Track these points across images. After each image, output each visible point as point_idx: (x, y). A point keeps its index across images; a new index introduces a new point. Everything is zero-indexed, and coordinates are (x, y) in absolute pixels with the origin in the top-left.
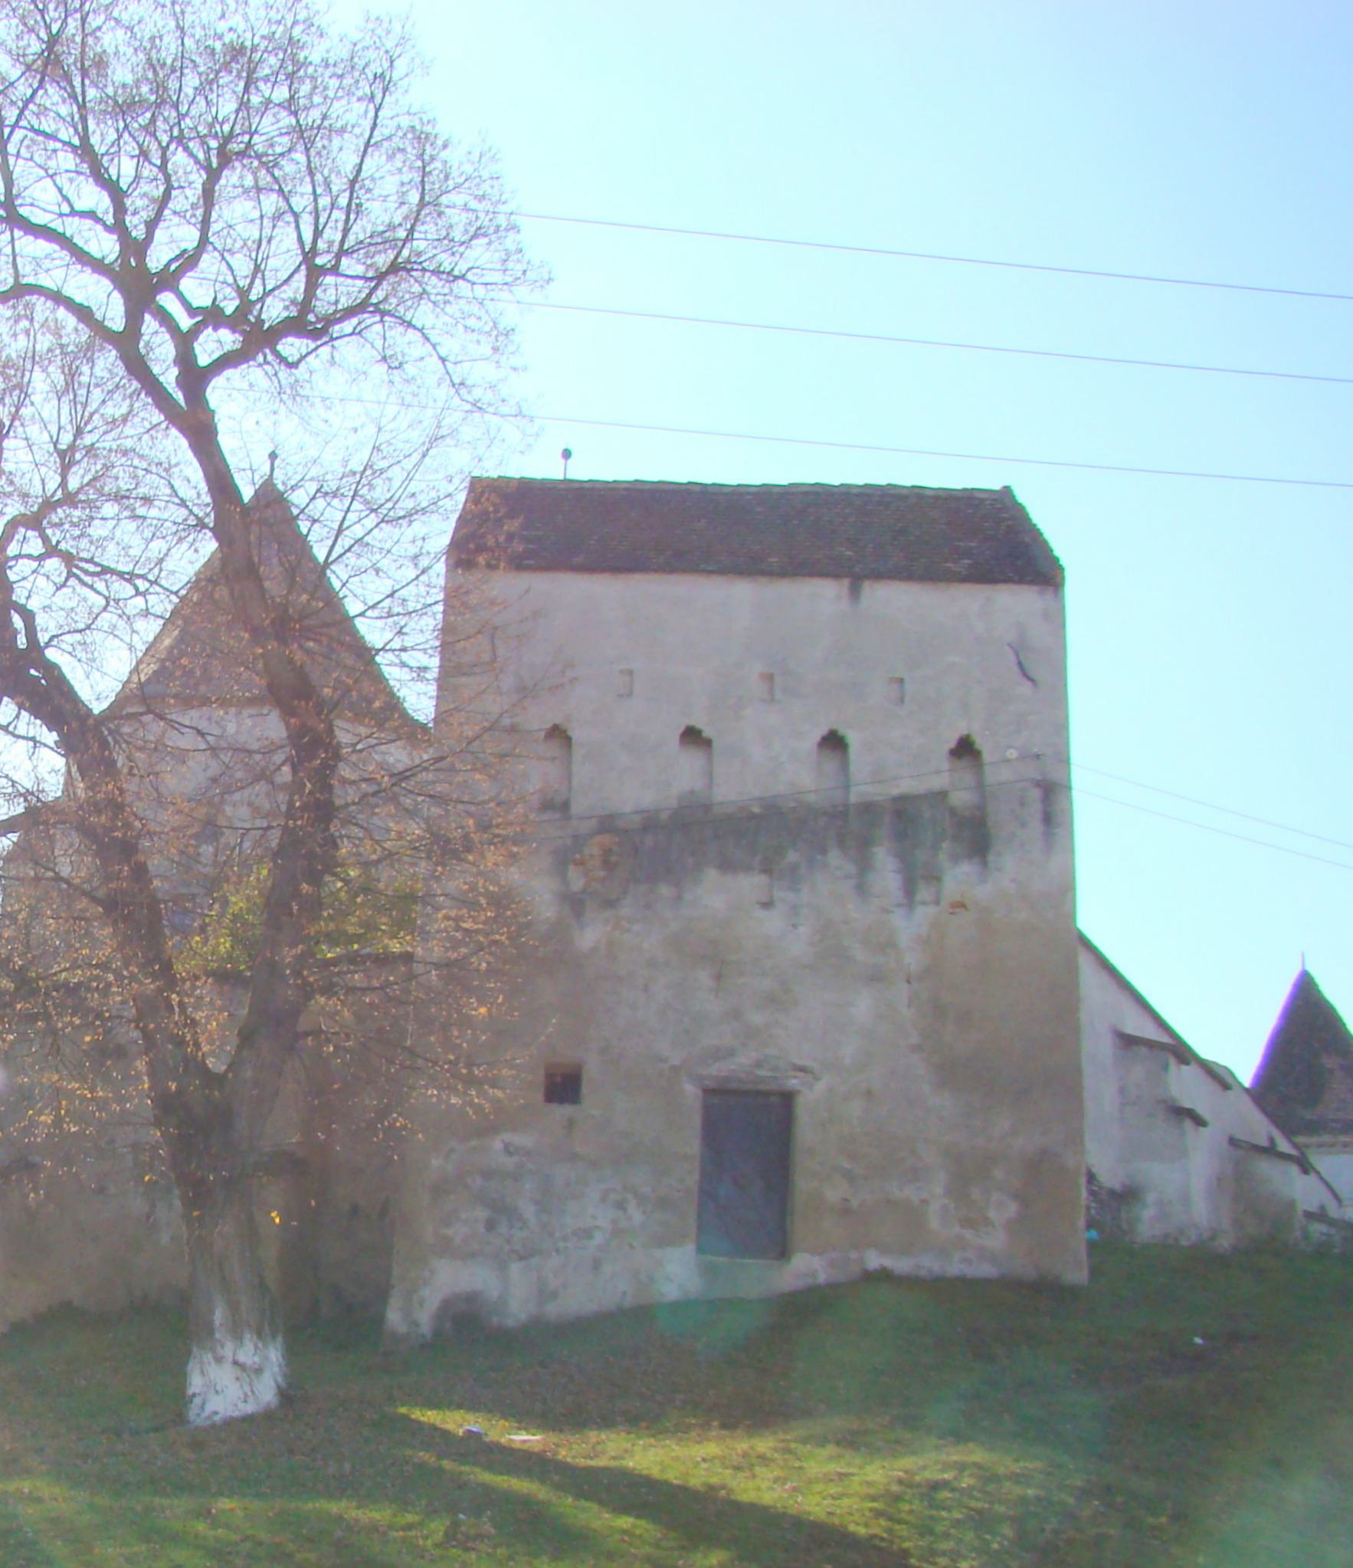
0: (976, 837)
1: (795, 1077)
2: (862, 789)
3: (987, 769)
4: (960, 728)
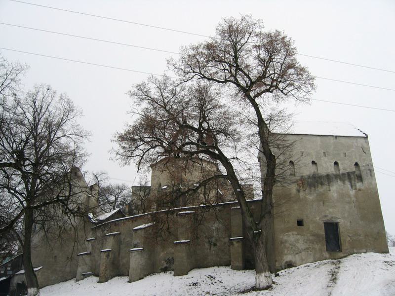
0: (360, 178)
1: (228, 230)
2: (342, 171)
3: (361, 168)
4: (356, 161)
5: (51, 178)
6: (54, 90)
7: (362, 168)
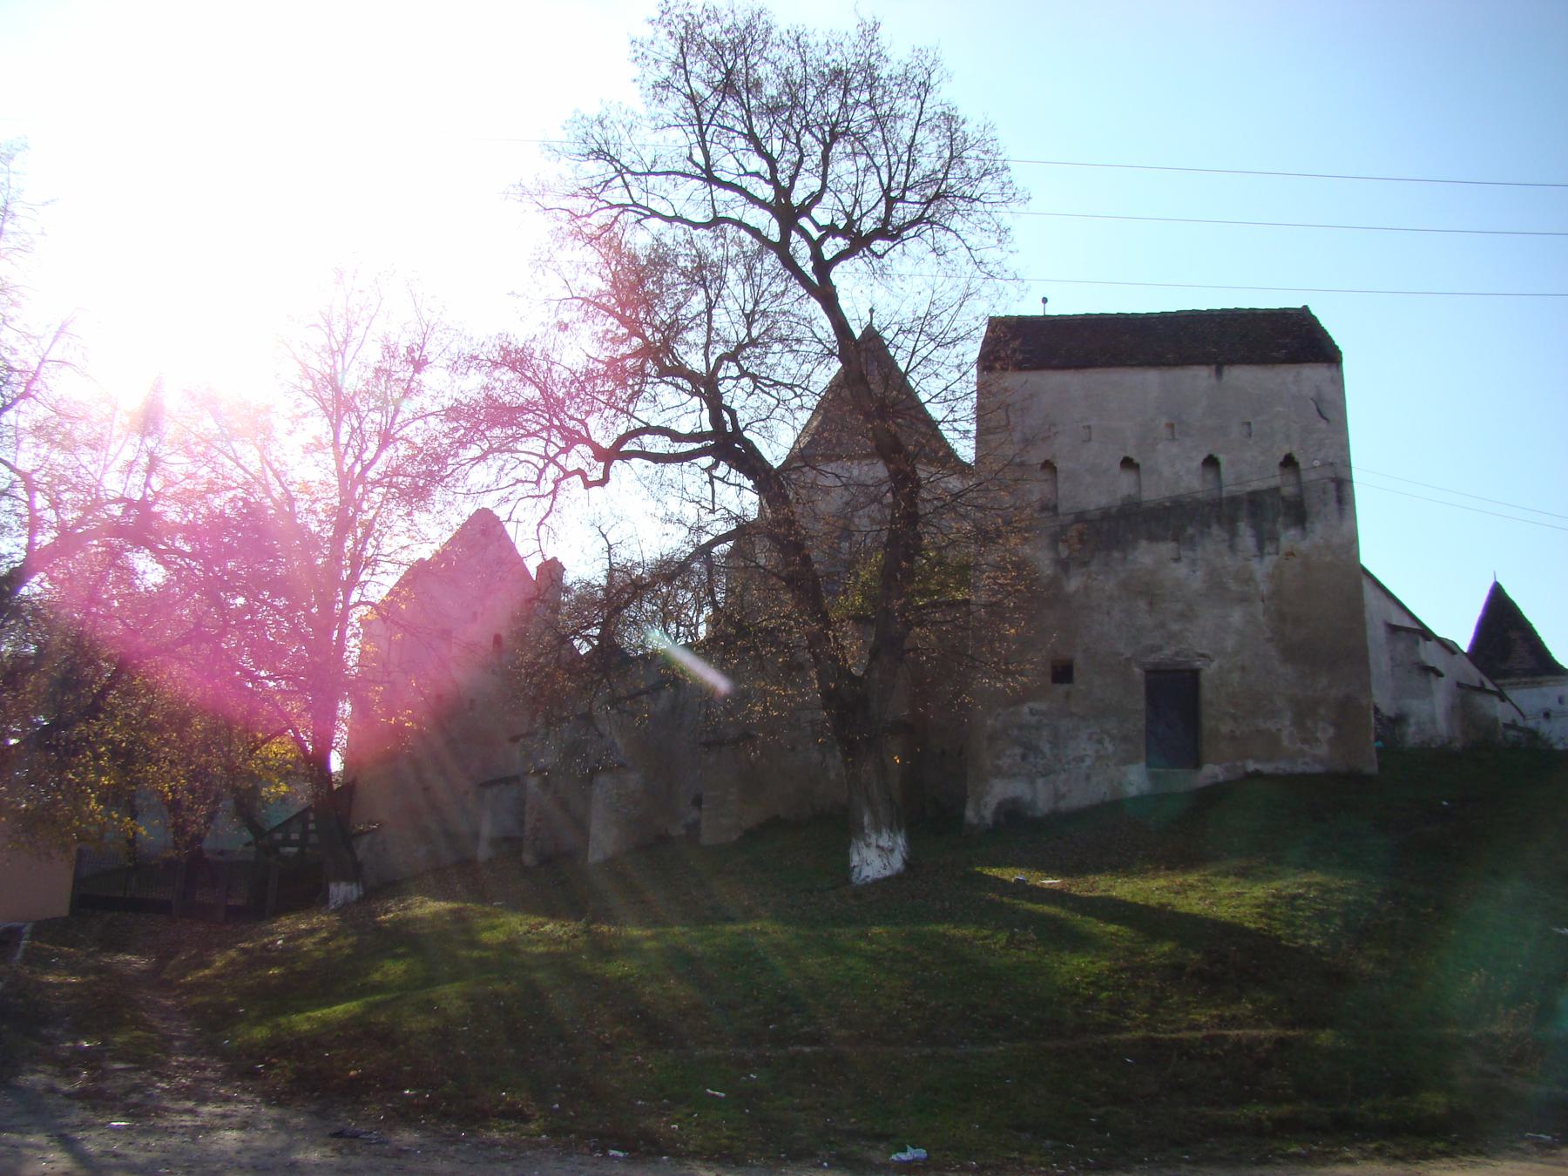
2: (1230, 488)
4: (1286, 450)
5: (779, 653)
6: (132, 402)
7: (1308, 476)
